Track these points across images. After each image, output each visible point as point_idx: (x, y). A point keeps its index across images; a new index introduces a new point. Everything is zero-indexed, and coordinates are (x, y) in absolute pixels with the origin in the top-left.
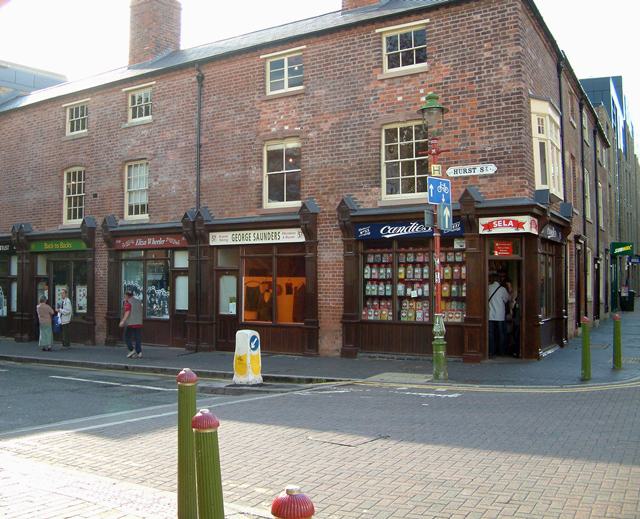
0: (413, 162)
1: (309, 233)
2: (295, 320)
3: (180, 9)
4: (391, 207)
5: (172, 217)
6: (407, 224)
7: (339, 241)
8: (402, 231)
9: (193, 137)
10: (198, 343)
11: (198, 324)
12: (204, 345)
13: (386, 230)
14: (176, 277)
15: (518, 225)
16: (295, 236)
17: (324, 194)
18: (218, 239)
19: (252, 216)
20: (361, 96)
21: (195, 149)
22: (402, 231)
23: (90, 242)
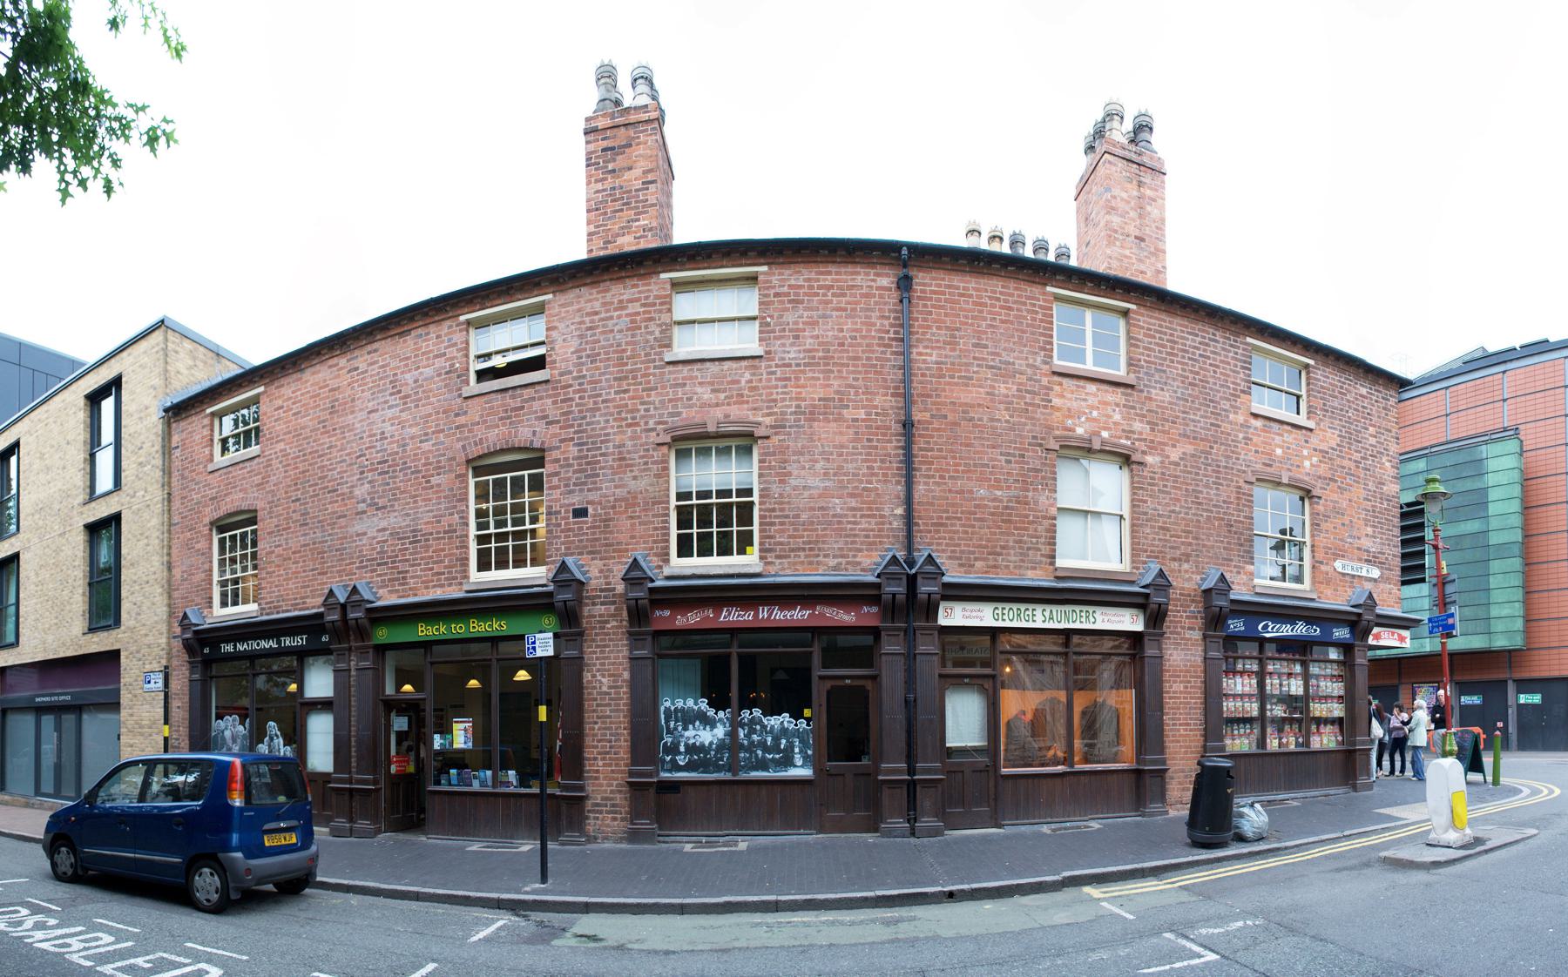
0: (731, 504)
1: (1156, 618)
2: (192, 749)
3: (68, 18)
4: (1284, 597)
5: (832, 562)
6: (1293, 623)
7: (1197, 635)
8: (1286, 630)
9: (886, 401)
10: (912, 820)
11: (914, 782)
12: (363, 824)
13: (1265, 627)
14: (982, 690)
15: (1402, 639)
16: (1129, 621)
17: (1174, 559)
18: (955, 615)
19: (1036, 577)
20: (1226, 427)
21: (898, 428)
22: (1286, 630)
23: (1156, 618)
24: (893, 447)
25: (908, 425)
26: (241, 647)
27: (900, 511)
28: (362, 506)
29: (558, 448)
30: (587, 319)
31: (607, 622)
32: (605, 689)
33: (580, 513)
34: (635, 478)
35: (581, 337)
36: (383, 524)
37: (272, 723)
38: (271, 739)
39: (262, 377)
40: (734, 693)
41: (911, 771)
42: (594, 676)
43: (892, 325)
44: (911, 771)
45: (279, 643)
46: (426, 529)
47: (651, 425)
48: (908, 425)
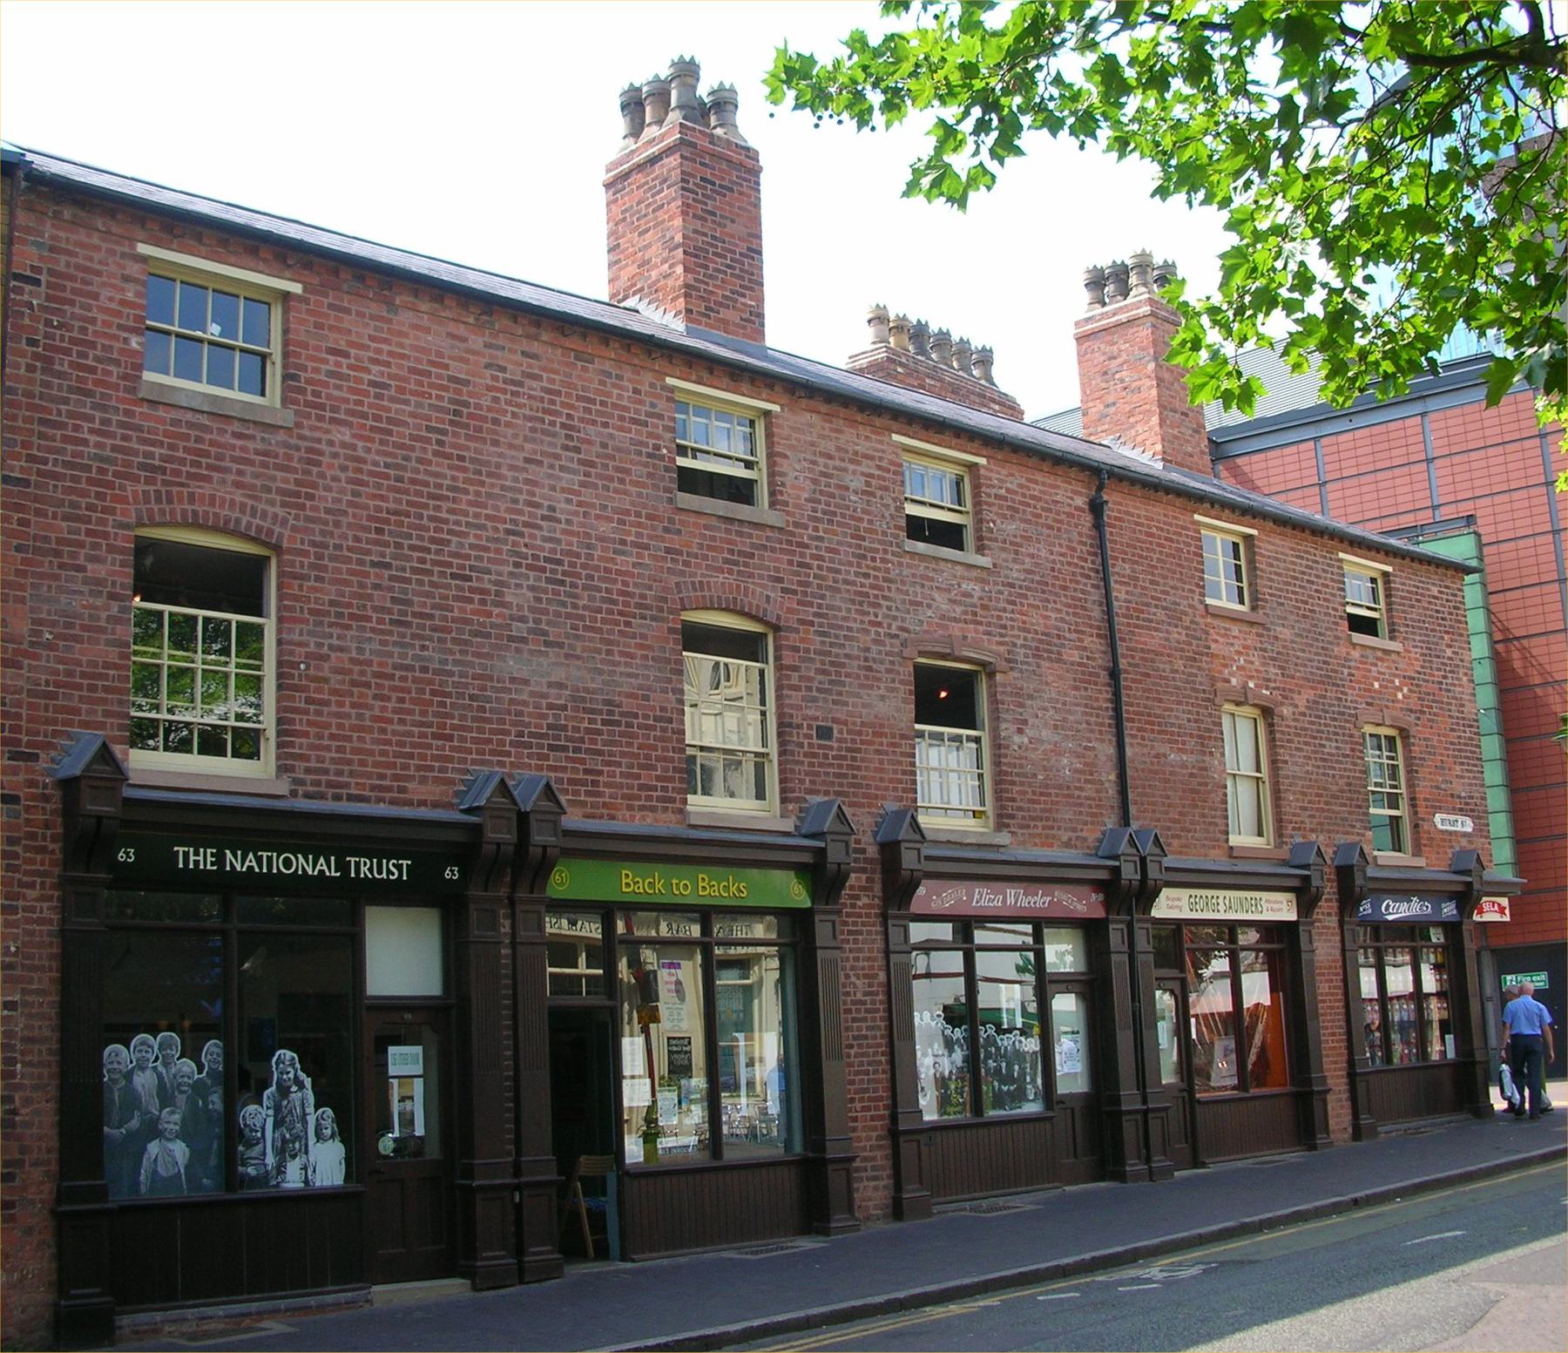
21: (1104, 676)
24: (1104, 697)
25: (1114, 674)
26: (235, 862)
27: (1113, 777)
28: (518, 629)
29: (797, 631)
30: (821, 460)
31: (858, 897)
32: (859, 996)
33: (825, 733)
34: (882, 698)
35: (815, 482)
36: (559, 675)
37: (288, 1054)
38: (284, 1091)
39: (307, 266)
40: (65, 1208)
41: (1145, 1102)
42: (847, 976)
43: (1090, 553)
44: (1145, 1102)
45: (343, 866)
46: (628, 705)
47: (894, 631)
48: (1114, 674)
